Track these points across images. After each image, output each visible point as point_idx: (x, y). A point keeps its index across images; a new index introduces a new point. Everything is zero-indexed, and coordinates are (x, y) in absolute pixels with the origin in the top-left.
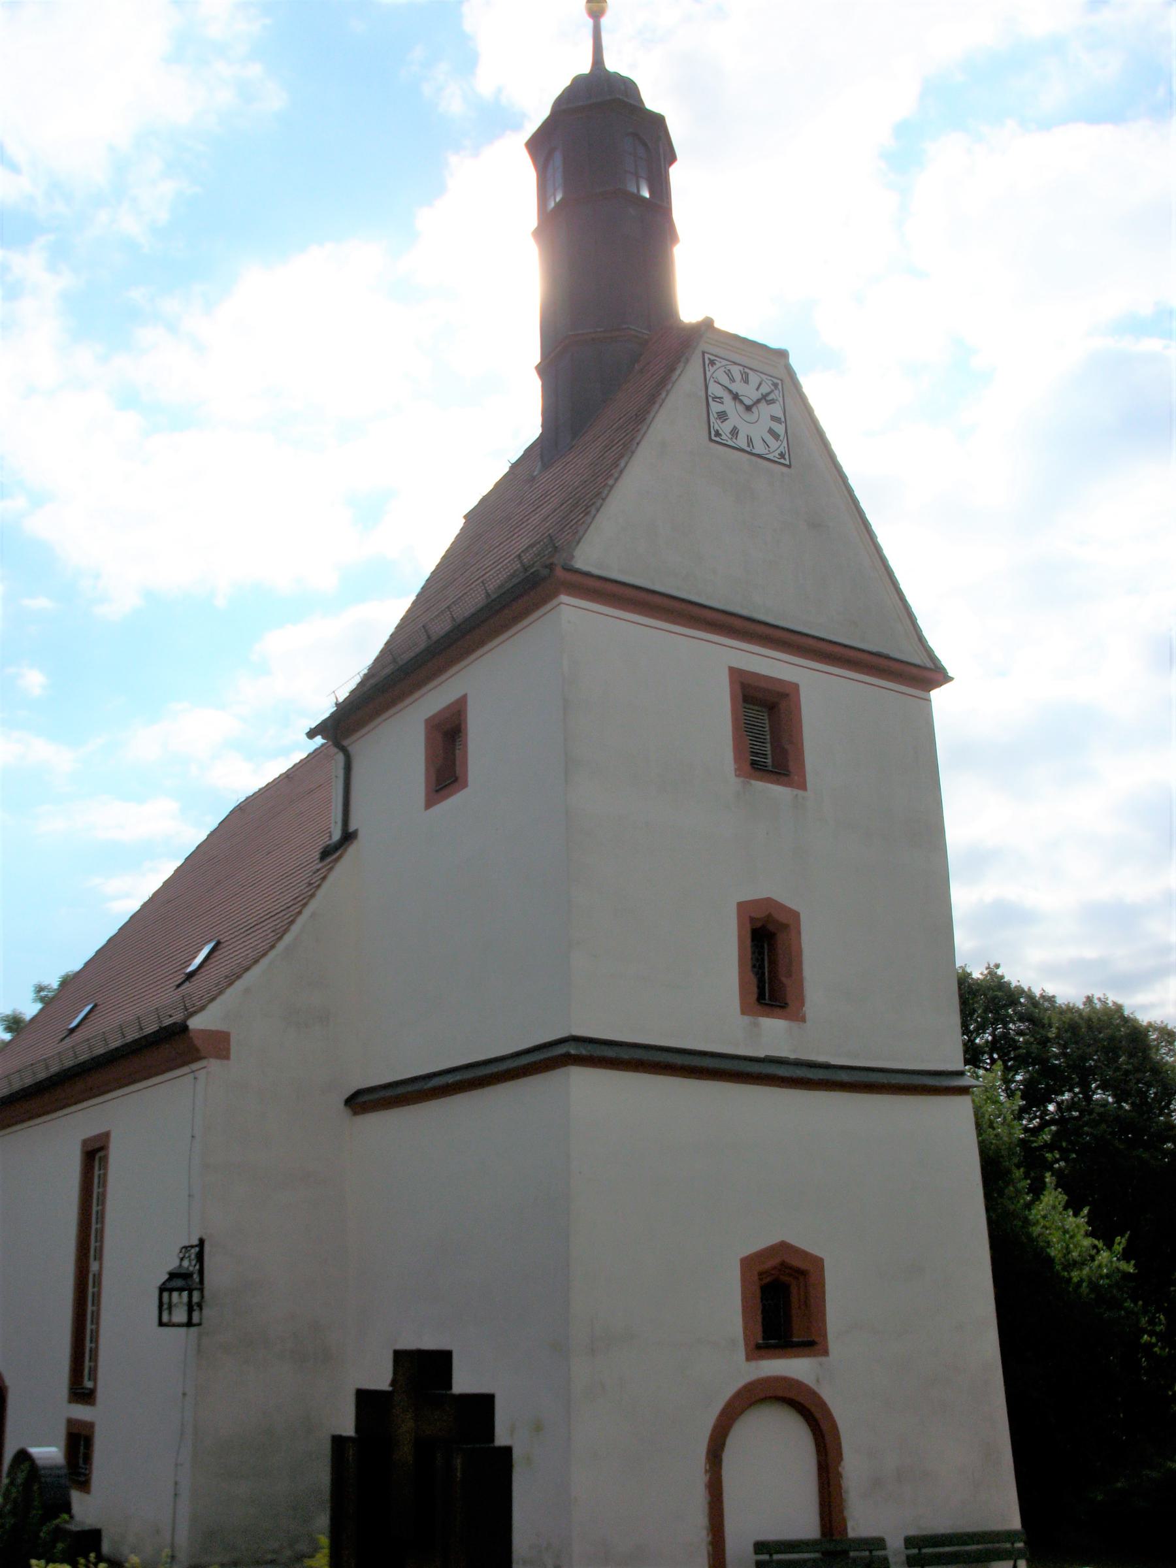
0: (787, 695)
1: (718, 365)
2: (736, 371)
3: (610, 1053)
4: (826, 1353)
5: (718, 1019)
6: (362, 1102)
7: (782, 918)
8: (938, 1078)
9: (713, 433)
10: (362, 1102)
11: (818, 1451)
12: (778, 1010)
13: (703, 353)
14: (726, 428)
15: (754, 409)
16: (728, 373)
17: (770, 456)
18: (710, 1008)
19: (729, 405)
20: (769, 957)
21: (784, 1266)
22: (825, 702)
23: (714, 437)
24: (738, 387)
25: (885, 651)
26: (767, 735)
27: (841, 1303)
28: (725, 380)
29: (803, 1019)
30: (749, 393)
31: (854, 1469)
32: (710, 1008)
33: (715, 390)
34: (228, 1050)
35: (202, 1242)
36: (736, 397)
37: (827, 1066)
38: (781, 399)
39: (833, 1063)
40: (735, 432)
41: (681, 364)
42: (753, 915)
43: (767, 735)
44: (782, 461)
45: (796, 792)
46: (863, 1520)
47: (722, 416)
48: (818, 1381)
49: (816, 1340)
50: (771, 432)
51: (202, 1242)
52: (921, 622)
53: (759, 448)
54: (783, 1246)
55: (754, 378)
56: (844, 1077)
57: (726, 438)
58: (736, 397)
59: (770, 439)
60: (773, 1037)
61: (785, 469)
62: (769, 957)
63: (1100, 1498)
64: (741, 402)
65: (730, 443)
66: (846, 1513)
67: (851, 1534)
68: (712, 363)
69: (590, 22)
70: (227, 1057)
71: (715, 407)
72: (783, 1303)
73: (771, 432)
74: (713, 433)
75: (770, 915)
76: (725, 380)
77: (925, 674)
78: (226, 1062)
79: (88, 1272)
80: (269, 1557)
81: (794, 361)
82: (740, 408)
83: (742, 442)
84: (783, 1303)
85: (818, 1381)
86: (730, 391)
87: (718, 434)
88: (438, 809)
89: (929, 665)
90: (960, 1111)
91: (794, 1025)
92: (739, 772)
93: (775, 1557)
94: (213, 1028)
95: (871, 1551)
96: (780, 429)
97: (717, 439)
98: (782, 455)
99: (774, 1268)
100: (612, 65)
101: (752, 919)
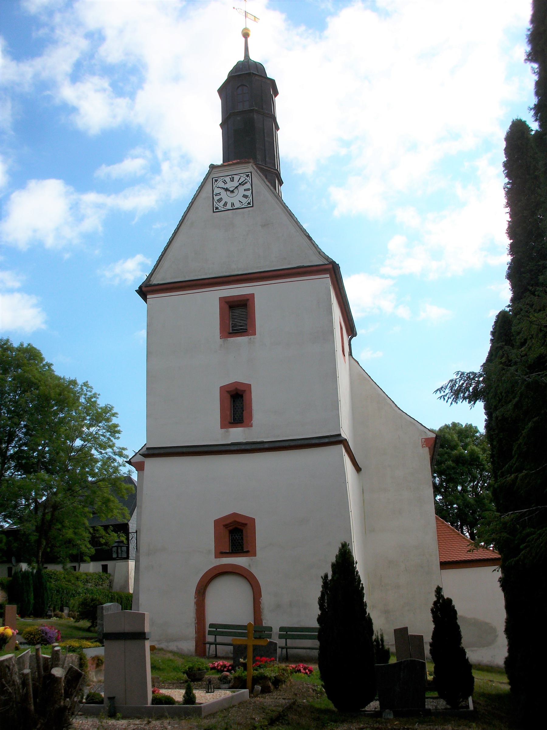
2: (228, 179)
4: (255, 555)
7: (242, 388)
12: (239, 425)
16: (225, 182)
17: (243, 206)
20: (236, 403)
27: (262, 535)
30: (230, 185)
31: (266, 600)
33: (217, 191)
34: (404, 628)
36: (226, 190)
40: (225, 204)
53: (237, 205)
54: (235, 514)
55: (236, 178)
58: (226, 190)
59: (222, 203)
60: (238, 434)
62: (236, 403)
63: (4, 446)
64: (229, 190)
66: (262, 617)
67: (264, 625)
69: (244, 39)
71: (216, 198)
72: (236, 535)
75: (236, 388)
76: (221, 184)
79: (39, 658)
82: (228, 193)
83: (229, 206)
84: (236, 535)
91: (246, 429)
96: (249, 193)
98: (217, 208)
101: (228, 392)
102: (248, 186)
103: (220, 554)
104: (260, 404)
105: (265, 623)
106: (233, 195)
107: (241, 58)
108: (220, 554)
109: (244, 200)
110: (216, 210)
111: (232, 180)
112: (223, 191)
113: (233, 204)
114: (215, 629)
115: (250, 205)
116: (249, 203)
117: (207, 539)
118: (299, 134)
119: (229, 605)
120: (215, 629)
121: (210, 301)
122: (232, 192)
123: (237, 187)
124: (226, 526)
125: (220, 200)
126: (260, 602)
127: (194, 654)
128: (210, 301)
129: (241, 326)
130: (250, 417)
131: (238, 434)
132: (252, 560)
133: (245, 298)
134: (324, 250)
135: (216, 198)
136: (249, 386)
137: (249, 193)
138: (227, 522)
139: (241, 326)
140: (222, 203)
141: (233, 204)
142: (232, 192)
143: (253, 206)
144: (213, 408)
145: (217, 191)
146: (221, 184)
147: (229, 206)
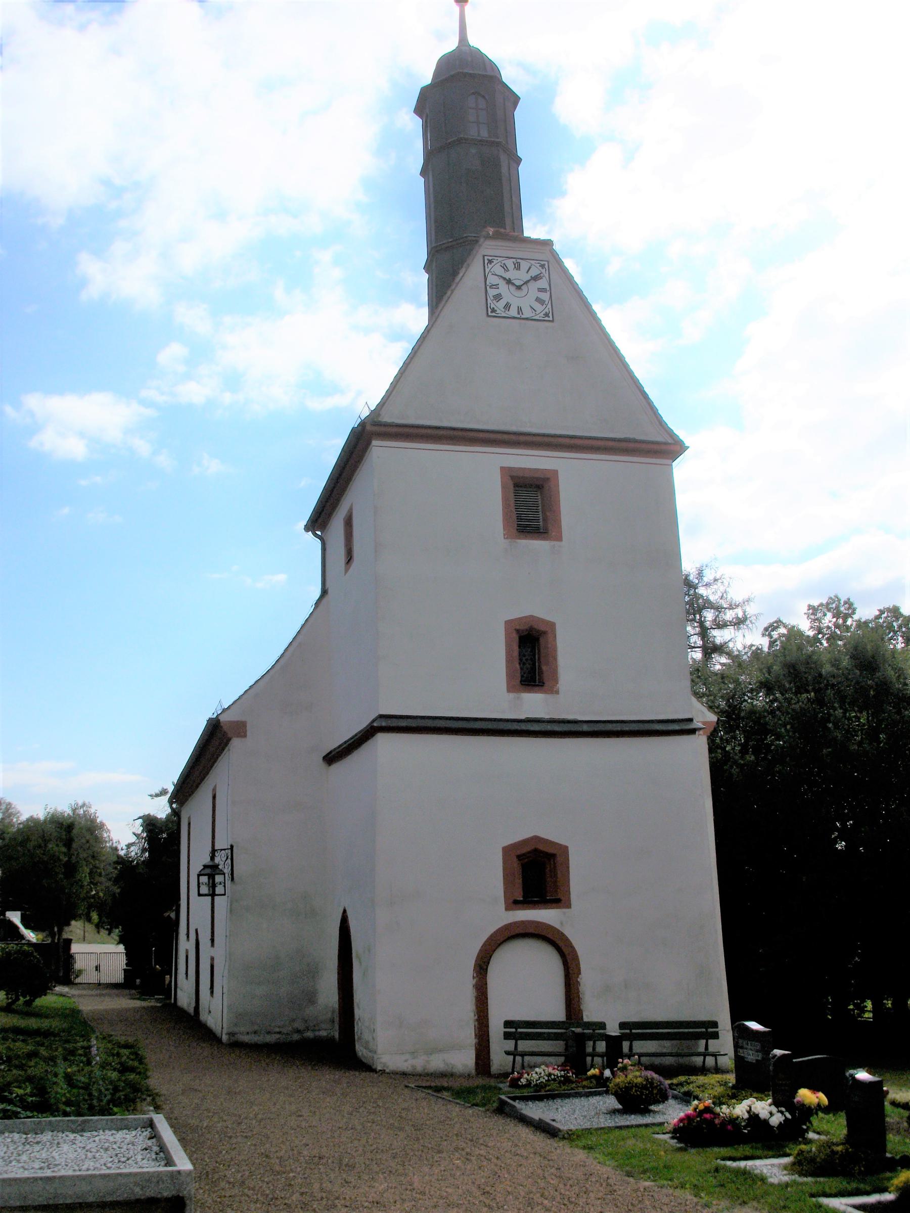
0: (548, 479)
1: (495, 262)
2: (510, 263)
3: (403, 723)
4: (568, 906)
5: (496, 698)
6: (332, 758)
7: (542, 628)
8: (666, 724)
9: (490, 310)
10: (332, 758)
11: (565, 969)
13: (484, 256)
14: (501, 305)
15: (524, 287)
16: (505, 268)
18: (489, 692)
19: (503, 288)
20: (531, 654)
21: (536, 851)
22: (577, 481)
23: (491, 313)
24: (512, 274)
25: (631, 436)
26: (531, 508)
27: (579, 875)
28: (500, 271)
29: (557, 692)
30: (519, 276)
31: (588, 980)
32: (489, 692)
33: (492, 280)
35: (232, 847)
36: (509, 282)
37: (576, 722)
38: (547, 275)
39: (580, 719)
40: (507, 306)
41: (463, 270)
42: (518, 627)
43: (531, 508)
44: (546, 318)
45: (553, 543)
46: (591, 1012)
47: (498, 297)
48: (562, 924)
49: (562, 898)
50: (538, 300)
51: (232, 847)
52: (661, 412)
53: (527, 313)
54: (536, 839)
55: (524, 265)
56: (585, 728)
57: (500, 311)
58: (509, 282)
60: (533, 705)
61: (550, 324)
62: (531, 654)
64: (513, 284)
65: (504, 315)
68: (490, 262)
70: (245, 736)
71: (492, 292)
72: (537, 873)
73: (538, 300)
74: (490, 310)
76: (500, 271)
77: (667, 448)
78: (243, 739)
80: (277, 1030)
81: (556, 247)
82: (512, 288)
83: (513, 312)
84: (537, 873)
85: (562, 924)
86: (505, 279)
87: (493, 311)
88: (348, 574)
89: (670, 441)
90: (699, 745)
92: (507, 536)
93: (519, 1030)
94: (235, 719)
95: (594, 1030)
96: (545, 296)
97: (494, 314)
99: (529, 852)
100: (474, 41)
101: (518, 631)
102: (543, 283)
103: (514, 904)
104: (569, 656)
105: (587, 1016)
106: (518, 293)
107: (451, 45)
108: (514, 904)
109: (539, 307)
110: (491, 313)
111: (518, 267)
112: (502, 284)
113: (520, 310)
114: (514, 1030)
115: (548, 317)
116: (547, 315)
117: (492, 878)
118: (572, 208)
119: (527, 988)
120: (514, 1030)
121: (486, 468)
122: (519, 288)
123: (526, 283)
124: (519, 857)
125: (498, 297)
126: (578, 983)
127: (473, 1072)
128: (486, 468)
129: (529, 520)
130: (556, 681)
131: (533, 705)
132: (564, 913)
133: (542, 476)
134: (666, 418)
135: (492, 292)
136: (507, 622)
137: (545, 296)
138: (524, 850)
139: (529, 520)
140: (501, 305)
141: (520, 310)
142: (519, 288)
143: (552, 321)
144: (496, 657)
145: (492, 280)
146: (499, 270)
147: (513, 312)
